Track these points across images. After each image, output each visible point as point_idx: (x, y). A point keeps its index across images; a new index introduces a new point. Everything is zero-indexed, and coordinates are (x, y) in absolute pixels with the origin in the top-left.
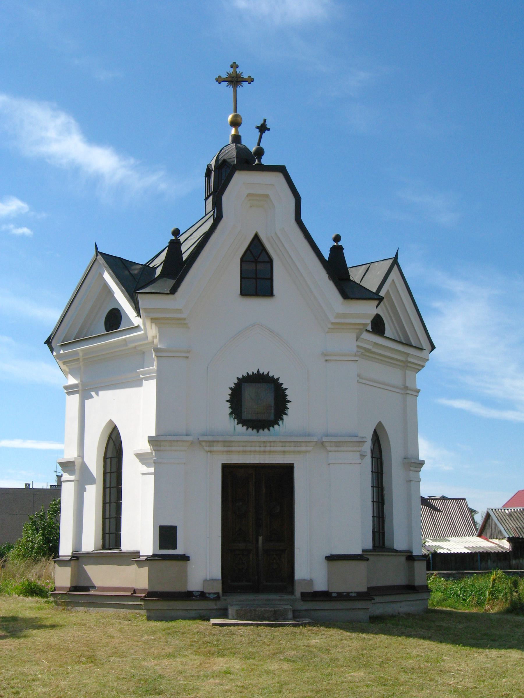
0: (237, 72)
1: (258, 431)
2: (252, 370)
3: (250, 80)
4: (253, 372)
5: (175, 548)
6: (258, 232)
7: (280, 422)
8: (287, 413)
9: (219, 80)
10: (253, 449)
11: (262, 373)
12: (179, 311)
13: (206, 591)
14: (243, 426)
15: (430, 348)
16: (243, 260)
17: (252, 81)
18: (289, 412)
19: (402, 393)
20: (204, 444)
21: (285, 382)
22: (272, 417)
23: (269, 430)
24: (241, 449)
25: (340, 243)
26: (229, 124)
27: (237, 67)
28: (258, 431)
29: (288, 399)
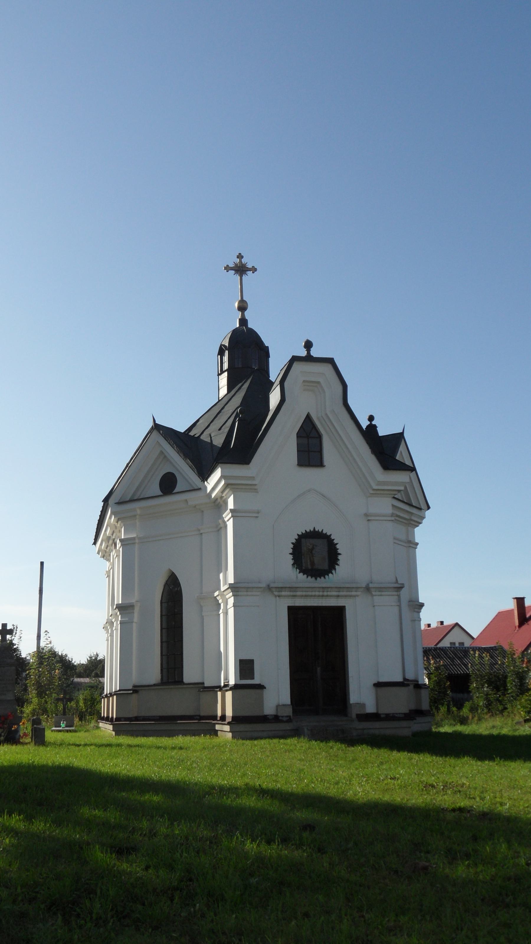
0: (242, 262)
1: (316, 579)
2: (309, 528)
3: (254, 270)
4: (310, 530)
5: (253, 678)
6: (310, 412)
7: (333, 571)
8: (338, 563)
9: (227, 268)
10: (313, 593)
11: (317, 530)
12: (253, 478)
13: (279, 714)
14: (304, 575)
15: (426, 508)
16: (299, 435)
17: (256, 271)
18: (340, 562)
19: (405, 546)
20: (274, 590)
21: (336, 538)
22: (326, 566)
23: (325, 578)
24: (304, 593)
25: (373, 423)
26: (237, 308)
27: (242, 257)
28: (316, 579)
29: (339, 552)
